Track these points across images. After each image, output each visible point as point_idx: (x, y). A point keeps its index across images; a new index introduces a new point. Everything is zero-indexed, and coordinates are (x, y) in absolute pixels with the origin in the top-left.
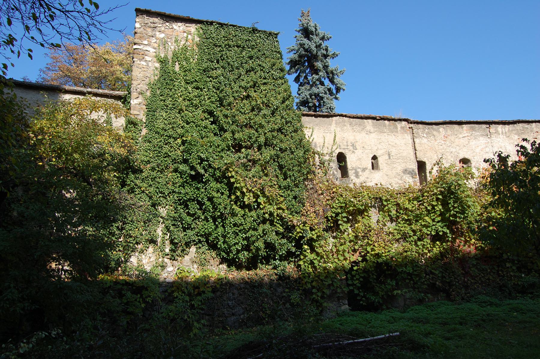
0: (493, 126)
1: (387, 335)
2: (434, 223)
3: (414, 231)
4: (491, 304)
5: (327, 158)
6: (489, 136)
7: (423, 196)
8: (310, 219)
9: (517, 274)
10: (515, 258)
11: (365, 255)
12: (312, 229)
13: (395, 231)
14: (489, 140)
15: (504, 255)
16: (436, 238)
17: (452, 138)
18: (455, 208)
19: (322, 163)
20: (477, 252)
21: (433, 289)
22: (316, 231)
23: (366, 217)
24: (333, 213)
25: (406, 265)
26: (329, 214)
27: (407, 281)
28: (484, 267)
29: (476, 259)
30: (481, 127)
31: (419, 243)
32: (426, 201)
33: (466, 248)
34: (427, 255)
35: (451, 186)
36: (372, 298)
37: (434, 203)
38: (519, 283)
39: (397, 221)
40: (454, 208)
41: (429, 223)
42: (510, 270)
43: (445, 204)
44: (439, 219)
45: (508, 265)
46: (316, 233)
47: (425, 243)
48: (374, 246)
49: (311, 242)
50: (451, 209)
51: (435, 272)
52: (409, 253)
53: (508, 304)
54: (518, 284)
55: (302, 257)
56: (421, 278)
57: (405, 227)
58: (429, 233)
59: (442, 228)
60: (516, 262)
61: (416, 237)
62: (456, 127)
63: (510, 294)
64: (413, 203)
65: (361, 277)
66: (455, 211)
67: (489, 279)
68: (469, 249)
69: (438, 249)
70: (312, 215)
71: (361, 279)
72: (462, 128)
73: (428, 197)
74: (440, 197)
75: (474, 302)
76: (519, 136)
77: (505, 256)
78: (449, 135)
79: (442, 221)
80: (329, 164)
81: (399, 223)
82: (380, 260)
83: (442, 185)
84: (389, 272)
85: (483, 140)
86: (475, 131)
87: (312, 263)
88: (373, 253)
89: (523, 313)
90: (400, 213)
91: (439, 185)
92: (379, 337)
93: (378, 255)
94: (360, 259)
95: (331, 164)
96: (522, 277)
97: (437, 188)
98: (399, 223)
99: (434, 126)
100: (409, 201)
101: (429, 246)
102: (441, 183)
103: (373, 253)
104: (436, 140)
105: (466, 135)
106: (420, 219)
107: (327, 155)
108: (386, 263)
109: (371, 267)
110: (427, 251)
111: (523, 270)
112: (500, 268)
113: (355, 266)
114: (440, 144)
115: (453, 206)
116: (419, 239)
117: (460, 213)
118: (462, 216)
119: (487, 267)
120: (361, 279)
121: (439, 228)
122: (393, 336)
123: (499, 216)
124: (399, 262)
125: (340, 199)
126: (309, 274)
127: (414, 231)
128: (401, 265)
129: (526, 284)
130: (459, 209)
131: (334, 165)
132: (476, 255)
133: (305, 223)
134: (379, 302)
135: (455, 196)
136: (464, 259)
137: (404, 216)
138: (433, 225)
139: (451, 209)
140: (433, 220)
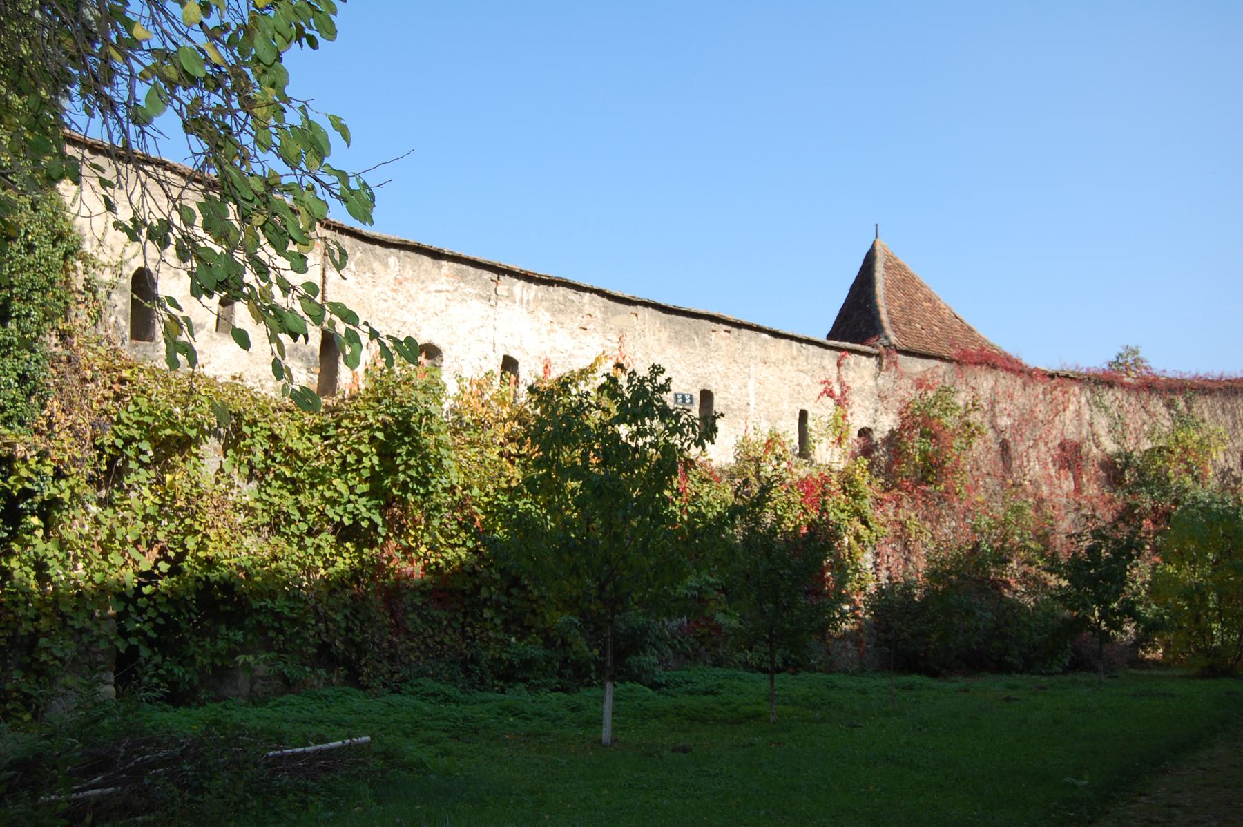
0: (505, 279)
1: (348, 741)
2: (353, 498)
3: (303, 511)
4: (448, 699)
5: (107, 276)
6: (492, 302)
7: (338, 426)
8: (58, 444)
9: (501, 636)
10: (504, 599)
11: (181, 557)
12: (59, 475)
13: (260, 506)
14: (491, 311)
15: (483, 590)
16: (344, 533)
17: (413, 287)
18: (409, 467)
19: (90, 288)
20: (427, 577)
21: (325, 656)
22: (72, 482)
23: (194, 459)
24: (118, 436)
25: (272, 595)
26: (108, 439)
27: (271, 634)
28: (435, 613)
29: (423, 593)
30: (480, 276)
31: (309, 541)
32: (342, 439)
33: (404, 564)
34: (317, 572)
35: (410, 415)
36: (176, 670)
37: (364, 448)
38: (504, 656)
39: (260, 479)
40: (406, 468)
41: (341, 495)
42: (488, 625)
43: (386, 453)
44: (365, 487)
45: (487, 613)
46: (71, 488)
47: (323, 544)
48: (206, 536)
49: (49, 509)
50: (402, 468)
51: (334, 616)
52: (283, 564)
53: (484, 702)
54: (500, 659)
55: (16, 548)
56: (304, 626)
57: (282, 497)
58: (337, 519)
59: (369, 510)
60: (504, 608)
61: (304, 527)
62: (427, 260)
63: (482, 681)
64: (310, 440)
65: (161, 615)
66: (410, 476)
67: (442, 643)
68: (411, 568)
69: (348, 561)
70: (63, 435)
71: (161, 621)
72: (440, 268)
73: (350, 430)
74: (380, 435)
75: (411, 693)
76: (553, 315)
77: (484, 593)
78: (406, 279)
79: (371, 494)
80: (109, 295)
81: (269, 485)
82: (214, 575)
83: (388, 407)
84: (228, 608)
85: (479, 307)
86: (466, 282)
87: (40, 566)
88: (201, 554)
89: (526, 719)
90: (274, 460)
91: (382, 408)
92: (332, 744)
93: (210, 563)
94: (164, 567)
95: (113, 296)
96: (509, 644)
97: (376, 413)
98: (269, 485)
99: (377, 247)
100: (301, 432)
101: (327, 550)
102: (385, 401)
103: (201, 554)
104: (374, 284)
105: (445, 287)
106: (321, 483)
107: (108, 270)
108: (227, 586)
109: (188, 591)
110: (320, 564)
111: (513, 627)
112: (469, 620)
113: (145, 585)
114: (384, 297)
115: (406, 463)
116: (310, 533)
117: (419, 483)
118: (422, 491)
119: (442, 614)
120: (161, 621)
121: (364, 510)
122: (357, 745)
123: (486, 500)
124: (257, 583)
125: (139, 400)
126: (28, 594)
127: (303, 511)
128: (259, 593)
129: (516, 661)
130: (418, 472)
131: (122, 301)
132: (424, 584)
133: (43, 455)
134: (190, 682)
135: (414, 440)
136: (396, 592)
137: (283, 469)
138: (349, 501)
139: (402, 468)
140: (352, 489)
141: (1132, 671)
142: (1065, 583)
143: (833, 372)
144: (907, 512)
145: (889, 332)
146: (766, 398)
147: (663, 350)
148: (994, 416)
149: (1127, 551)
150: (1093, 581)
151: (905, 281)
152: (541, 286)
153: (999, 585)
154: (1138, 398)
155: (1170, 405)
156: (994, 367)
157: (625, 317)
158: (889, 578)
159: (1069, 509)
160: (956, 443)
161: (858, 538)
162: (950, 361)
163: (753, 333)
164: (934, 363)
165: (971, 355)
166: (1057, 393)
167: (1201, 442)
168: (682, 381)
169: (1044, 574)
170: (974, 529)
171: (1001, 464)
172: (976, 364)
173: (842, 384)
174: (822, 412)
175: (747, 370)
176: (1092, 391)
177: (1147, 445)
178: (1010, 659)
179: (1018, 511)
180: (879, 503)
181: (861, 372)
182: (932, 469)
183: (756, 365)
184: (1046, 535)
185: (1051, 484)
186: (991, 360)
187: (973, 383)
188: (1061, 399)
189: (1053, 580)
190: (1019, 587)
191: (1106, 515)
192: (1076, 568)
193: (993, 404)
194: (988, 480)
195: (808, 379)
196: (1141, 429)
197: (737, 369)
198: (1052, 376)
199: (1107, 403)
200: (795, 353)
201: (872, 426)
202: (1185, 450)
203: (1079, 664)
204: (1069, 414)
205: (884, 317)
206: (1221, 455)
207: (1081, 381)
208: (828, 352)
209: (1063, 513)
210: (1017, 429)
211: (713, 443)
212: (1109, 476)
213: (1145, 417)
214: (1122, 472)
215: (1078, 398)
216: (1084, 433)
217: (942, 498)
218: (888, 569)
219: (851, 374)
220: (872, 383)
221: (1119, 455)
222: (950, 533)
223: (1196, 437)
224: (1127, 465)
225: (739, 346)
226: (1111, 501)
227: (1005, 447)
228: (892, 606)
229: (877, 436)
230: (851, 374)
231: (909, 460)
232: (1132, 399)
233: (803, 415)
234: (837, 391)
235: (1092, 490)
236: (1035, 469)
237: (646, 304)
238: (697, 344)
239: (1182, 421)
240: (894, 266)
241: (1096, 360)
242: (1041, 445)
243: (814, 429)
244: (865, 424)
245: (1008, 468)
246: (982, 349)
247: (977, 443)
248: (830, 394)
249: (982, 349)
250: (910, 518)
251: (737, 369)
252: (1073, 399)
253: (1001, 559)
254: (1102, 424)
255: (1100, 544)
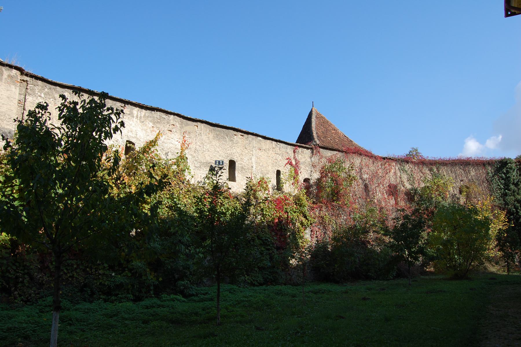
76: (154, 124)
99: (58, 87)
141: (422, 277)
142: (392, 240)
143: (292, 155)
144: (325, 212)
145: (316, 140)
146: (261, 165)
147: (211, 142)
148: (361, 174)
149: (419, 225)
150: (405, 239)
151: (323, 122)
152: (148, 111)
153: (365, 243)
154: (418, 168)
155: (431, 170)
156: (361, 154)
157: (192, 127)
158: (317, 241)
159: (392, 209)
160: (344, 183)
161: (302, 223)
162: (342, 152)
163: (254, 137)
164: (335, 152)
165: (351, 150)
166: (386, 165)
167: (444, 183)
168: (220, 156)
169: (384, 237)
170: (354, 219)
171: (365, 193)
172: (353, 153)
173: (296, 160)
174: (286, 171)
175: (251, 152)
176: (400, 164)
177: (423, 185)
178: (371, 274)
179: (371, 211)
180: (312, 209)
181: (304, 155)
182: (336, 194)
183: (256, 150)
184: (384, 221)
185: (386, 202)
186: (359, 152)
187: (352, 161)
188: (388, 168)
189: (387, 239)
190: (374, 243)
191: (408, 212)
192: (397, 233)
193: (361, 169)
194: (360, 200)
195: (280, 157)
196: (421, 180)
197: (247, 152)
198: (384, 158)
199: (406, 169)
200: (274, 146)
201: (310, 178)
202: (438, 186)
203: (400, 275)
204: (392, 174)
205: (315, 134)
206: (452, 189)
207: (396, 160)
208: (289, 146)
209: (391, 213)
210: (371, 180)
211: (124, 127)
212: (408, 198)
213: (422, 175)
214: (414, 196)
215: (395, 167)
216: (398, 181)
217: (340, 207)
218: (317, 237)
219: (300, 156)
220: (309, 160)
221: (412, 189)
222: (344, 221)
223: (442, 182)
224: (415, 193)
225: (248, 142)
226: (410, 208)
227: (366, 186)
228: (319, 251)
229: (312, 182)
230: (300, 156)
231: (325, 192)
232: (416, 168)
233: (278, 173)
234: (294, 163)
235: (402, 204)
236: (379, 195)
237: (202, 122)
238: (227, 140)
239: (435, 176)
240: (319, 117)
241: (401, 152)
242: (381, 186)
243: (283, 178)
244: (306, 177)
245: (368, 195)
246: (356, 148)
247: (354, 183)
248: (291, 164)
249: (356, 148)
250: (325, 215)
251: (247, 152)
252: (393, 167)
253: (366, 232)
254: (405, 177)
255: (407, 222)
